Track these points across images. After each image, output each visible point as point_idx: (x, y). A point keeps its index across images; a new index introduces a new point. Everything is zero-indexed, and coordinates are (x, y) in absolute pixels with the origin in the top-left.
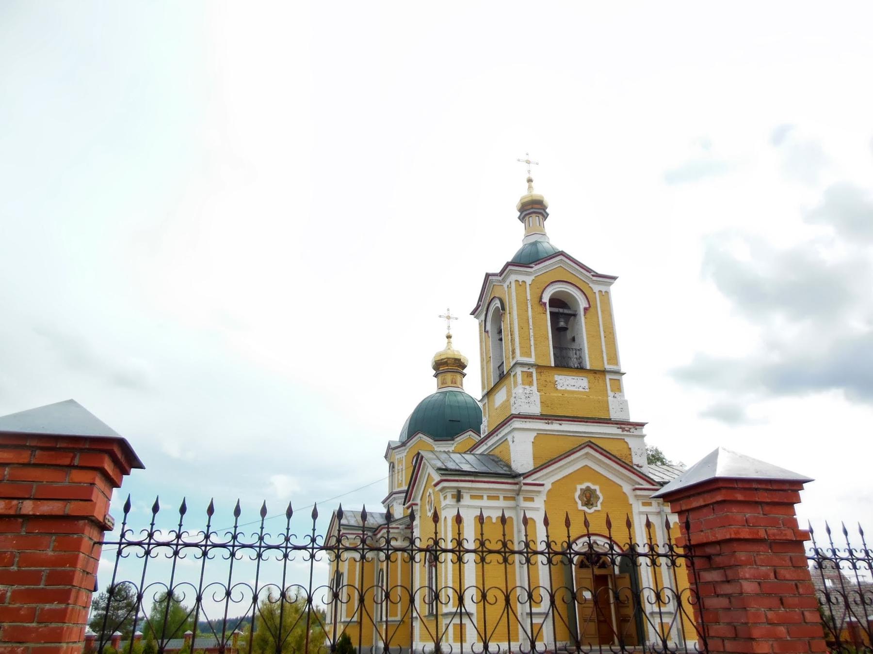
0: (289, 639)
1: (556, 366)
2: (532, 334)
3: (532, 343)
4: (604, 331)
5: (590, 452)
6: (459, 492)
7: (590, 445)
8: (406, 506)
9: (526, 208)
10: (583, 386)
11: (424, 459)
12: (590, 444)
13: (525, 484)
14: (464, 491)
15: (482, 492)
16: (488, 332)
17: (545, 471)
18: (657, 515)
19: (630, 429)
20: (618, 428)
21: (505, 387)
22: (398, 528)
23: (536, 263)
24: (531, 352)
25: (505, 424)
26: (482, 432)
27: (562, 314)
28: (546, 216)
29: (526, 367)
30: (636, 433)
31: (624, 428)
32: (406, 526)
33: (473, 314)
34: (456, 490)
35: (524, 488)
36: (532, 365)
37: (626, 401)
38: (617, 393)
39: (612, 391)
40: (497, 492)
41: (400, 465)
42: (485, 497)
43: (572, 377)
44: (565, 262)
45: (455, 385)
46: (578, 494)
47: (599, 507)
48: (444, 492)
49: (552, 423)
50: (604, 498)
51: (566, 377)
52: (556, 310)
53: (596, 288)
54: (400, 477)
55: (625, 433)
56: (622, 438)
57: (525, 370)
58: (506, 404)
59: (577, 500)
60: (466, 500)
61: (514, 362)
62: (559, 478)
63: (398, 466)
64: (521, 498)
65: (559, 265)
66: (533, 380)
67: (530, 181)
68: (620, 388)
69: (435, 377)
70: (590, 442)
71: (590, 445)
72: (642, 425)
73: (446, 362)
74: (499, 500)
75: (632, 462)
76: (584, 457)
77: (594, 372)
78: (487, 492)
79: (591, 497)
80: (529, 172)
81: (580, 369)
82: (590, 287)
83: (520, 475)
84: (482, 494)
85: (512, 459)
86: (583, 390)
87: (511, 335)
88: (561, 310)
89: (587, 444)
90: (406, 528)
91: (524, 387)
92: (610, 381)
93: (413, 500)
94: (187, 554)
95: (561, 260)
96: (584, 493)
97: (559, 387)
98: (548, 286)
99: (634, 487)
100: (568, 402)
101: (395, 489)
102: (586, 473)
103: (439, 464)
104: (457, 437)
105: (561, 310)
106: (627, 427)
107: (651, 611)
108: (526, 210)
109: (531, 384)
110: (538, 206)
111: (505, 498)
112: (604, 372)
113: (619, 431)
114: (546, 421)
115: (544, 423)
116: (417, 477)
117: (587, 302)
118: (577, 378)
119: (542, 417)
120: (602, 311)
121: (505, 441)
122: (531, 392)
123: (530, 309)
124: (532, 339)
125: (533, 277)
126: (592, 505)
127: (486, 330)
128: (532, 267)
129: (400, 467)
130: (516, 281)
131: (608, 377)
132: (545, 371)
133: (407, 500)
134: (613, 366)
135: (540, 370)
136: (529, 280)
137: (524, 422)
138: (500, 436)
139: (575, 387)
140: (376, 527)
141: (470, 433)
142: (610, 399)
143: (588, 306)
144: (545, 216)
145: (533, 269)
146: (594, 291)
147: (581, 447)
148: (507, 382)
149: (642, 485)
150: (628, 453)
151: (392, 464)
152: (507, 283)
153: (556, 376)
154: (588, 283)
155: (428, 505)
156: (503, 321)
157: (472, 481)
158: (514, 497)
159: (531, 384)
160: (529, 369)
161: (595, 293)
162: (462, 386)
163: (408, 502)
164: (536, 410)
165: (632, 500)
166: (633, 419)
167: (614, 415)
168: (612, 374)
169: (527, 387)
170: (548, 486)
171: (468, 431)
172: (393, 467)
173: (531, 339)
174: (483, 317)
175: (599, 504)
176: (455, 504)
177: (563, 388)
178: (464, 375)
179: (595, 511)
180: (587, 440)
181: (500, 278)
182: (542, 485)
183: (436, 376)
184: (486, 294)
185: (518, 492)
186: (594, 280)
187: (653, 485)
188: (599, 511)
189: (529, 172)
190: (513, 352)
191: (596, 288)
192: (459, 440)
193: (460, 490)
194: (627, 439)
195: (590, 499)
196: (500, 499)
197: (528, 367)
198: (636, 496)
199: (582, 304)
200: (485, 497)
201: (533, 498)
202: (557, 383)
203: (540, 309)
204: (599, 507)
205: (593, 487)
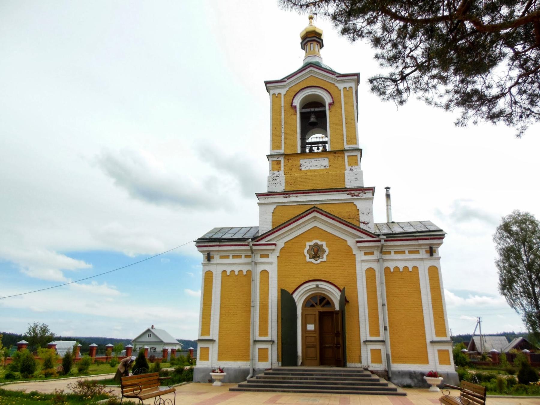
0: (462, 361)
2: (283, 131)
3: (283, 138)
5: (316, 215)
6: (431, 248)
9: (309, 36)
10: (324, 165)
14: (213, 253)
15: (404, 248)
16: (295, 107)
19: (360, 193)
20: (348, 194)
24: (281, 145)
27: (313, 112)
30: (365, 196)
31: (354, 194)
34: (428, 247)
36: (281, 155)
37: (362, 172)
38: (353, 166)
39: (349, 165)
40: (240, 253)
42: (231, 257)
43: (316, 159)
44: (315, 71)
49: (290, 197)
51: (309, 160)
53: (341, 86)
55: (355, 197)
57: (275, 160)
59: (306, 254)
60: (216, 260)
62: (291, 238)
65: (310, 75)
70: (315, 207)
71: (314, 209)
74: (405, 253)
77: (334, 152)
79: (318, 251)
82: (336, 86)
89: (313, 210)
91: (273, 172)
96: (312, 248)
100: (309, 179)
106: (356, 193)
107: (365, 340)
111: (246, 256)
112: (342, 151)
113: (349, 197)
114: (285, 196)
115: (283, 197)
119: (286, 193)
120: (346, 103)
123: (283, 113)
126: (319, 257)
131: (346, 154)
132: (292, 158)
134: (352, 145)
135: (287, 158)
137: (267, 199)
139: (317, 166)
142: (347, 172)
145: (287, 82)
149: (363, 238)
154: (335, 83)
157: (219, 246)
158: (251, 255)
159: (279, 169)
166: (366, 185)
167: (348, 185)
168: (351, 151)
169: (276, 172)
170: (281, 244)
175: (325, 256)
176: (429, 257)
177: (307, 169)
179: (321, 262)
180: (312, 206)
182: (275, 245)
186: (338, 80)
187: (373, 237)
188: (325, 261)
191: (341, 86)
193: (432, 246)
194: (356, 203)
195: (317, 252)
197: (278, 157)
198: (359, 247)
199: (328, 100)
200: (407, 252)
201: (390, 252)
202: (302, 166)
204: (325, 259)
205: (320, 243)
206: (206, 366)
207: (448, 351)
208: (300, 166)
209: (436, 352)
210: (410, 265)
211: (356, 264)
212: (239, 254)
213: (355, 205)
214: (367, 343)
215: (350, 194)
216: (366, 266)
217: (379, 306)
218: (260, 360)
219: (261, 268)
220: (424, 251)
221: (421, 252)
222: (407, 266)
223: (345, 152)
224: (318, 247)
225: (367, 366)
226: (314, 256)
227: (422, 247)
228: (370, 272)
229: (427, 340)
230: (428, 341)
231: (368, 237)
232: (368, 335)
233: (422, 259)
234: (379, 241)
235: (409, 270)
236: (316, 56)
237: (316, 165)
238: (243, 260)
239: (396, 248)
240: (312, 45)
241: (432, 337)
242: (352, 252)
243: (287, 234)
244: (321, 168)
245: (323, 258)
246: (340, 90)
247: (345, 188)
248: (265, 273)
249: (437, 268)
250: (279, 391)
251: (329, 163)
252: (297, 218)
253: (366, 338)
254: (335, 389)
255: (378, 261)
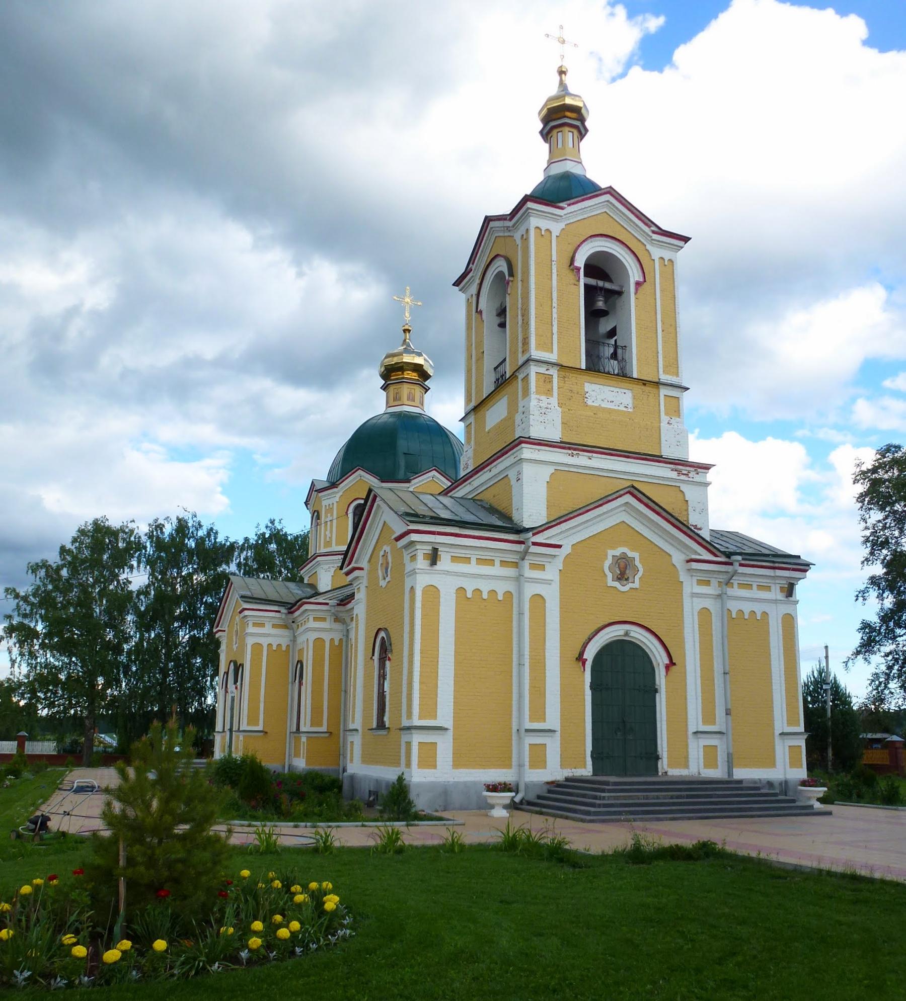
1: (588, 369)
2: (555, 315)
4: (662, 321)
6: (435, 551)
7: (633, 491)
8: (345, 570)
9: (554, 116)
10: (625, 403)
11: (378, 499)
12: (632, 490)
13: (534, 544)
15: (752, 580)
16: (481, 312)
17: (564, 526)
18: (716, 599)
21: (506, 398)
22: (327, 604)
23: (568, 202)
25: (506, 453)
26: (462, 467)
27: (601, 289)
28: (583, 131)
29: (543, 367)
30: (697, 478)
32: (338, 602)
33: (458, 286)
34: (430, 548)
35: (533, 549)
36: (553, 364)
39: (666, 414)
40: (768, 581)
41: (329, 515)
42: (473, 561)
43: (612, 389)
45: (400, 403)
46: (608, 562)
47: (636, 585)
48: (410, 551)
50: (644, 571)
52: (592, 282)
53: (657, 253)
54: (328, 533)
55: (683, 477)
56: (678, 484)
58: (509, 422)
61: (525, 358)
63: (326, 517)
64: (526, 563)
66: (552, 387)
67: (562, 72)
68: (679, 411)
69: (384, 390)
70: (633, 487)
71: (633, 491)
72: (707, 467)
73: (403, 366)
74: (494, 565)
75: (688, 521)
76: (623, 508)
77: (644, 383)
78: (476, 553)
79: (626, 568)
80: (563, 57)
81: (624, 375)
83: (527, 530)
84: (469, 556)
85: (513, 506)
86: (625, 409)
87: (523, 316)
88: (601, 283)
90: (338, 605)
91: (538, 396)
92: (665, 400)
93: (356, 562)
94: (854, 602)
95: (608, 201)
97: (590, 402)
98: (584, 241)
99: (688, 558)
101: (319, 550)
102: (622, 532)
103: (403, 509)
104: (414, 479)
105: (601, 283)
107: (695, 730)
108: (552, 120)
109: (549, 392)
110: (574, 115)
111: (504, 563)
112: (658, 384)
113: (674, 475)
114: (570, 452)
116: (365, 527)
117: (641, 274)
118: (618, 390)
119: (562, 445)
121: (505, 477)
122: (549, 406)
124: (555, 323)
125: (562, 225)
126: (627, 580)
127: (479, 310)
128: (562, 208)
129: (329, 518)
130: (537, 228)
133: (347, 562)
136: (556, 228)
137: (537, 451)
138: (495, 471)
140: (293, 602)
141: (360, 472)
142: (664, 425)
143: (641, 280)
144: (582, 132)
145: (564, 212)
146: (653, 258)
147: (618, 494)
148: (509, 389)
149: (700, 555)
150: (685, 508)
151: (316, 514)
152: (522, 230)
153: (587, 385)
154: (645, 243)
155: (382, 569)
156: (511, 288)
160: (547, 370)
161: (654, 260)
162: (422, 405)
163: (348, 565)
164: (555, 435)
165: (683, 577)
166: (693, 458)
167: (666, 452)
169: (543, 398)
170: (566, 550)
171: (431, 471)
172: (318, 518)
173: (553, 323)
174: (473, 289)
175: (637, 578)
178: (427, 390)
180: (629, 484)
181: (510, 224)
182: (559, 546)
183: (385, 388)
184: (482, 251)
185: (524, 555)
187: (716, 556)
189: (563, 57)
190: (526, 342)
191: (657, 253)
192: (418, 483)
194: (684, 488)
195: (625, 571)
196: (734, 586)
197: (547, 367)
199: (634, 275)
200: (473, 561)
202: (587, 395)
203: (571, 276)
205: (630, 554)
206: (433, 779)
207: (258, 725)
208: (584, 395)
209: (787, 749)
210: (758, 608)
211: (682, 599)
212: (490, 558)
213: (681, 491)
214: (700, 735)
215: (676, 471)
216: (699, 604)
217: (716, 674)
218: (533, 766)
219: (530, 590)
220: (778, 586)
221: (773, 588)
222: (543, 593)
223: (661, 386)
224: (627, 560)
225: (697, 774)
226: (619, 576)
227: (777, 582)
228: (704, 613)
229: (775, 731)
230: (777, 732)
231: (709, 554)
232: (785, 724)
233: (776, 601)
234: (731, 564)
235: (756, 617)
236: (566, 159)
237: (612, 400)
238: (496, 570)
239: (741, 579)
240: (560, 134)
241: (783, 727)
242: (679, 578)
243: (582, 527)
244: (619, 408)
245: (634, 583)
246: (654, 260)
247: (661, 457)
248: (538, 599)
249: (793, 618)
250: (667, 819)
251: (633, 403)
252: (600, 502)
253: (697, 728)
254: (729, 812)
255: (719, 596)
